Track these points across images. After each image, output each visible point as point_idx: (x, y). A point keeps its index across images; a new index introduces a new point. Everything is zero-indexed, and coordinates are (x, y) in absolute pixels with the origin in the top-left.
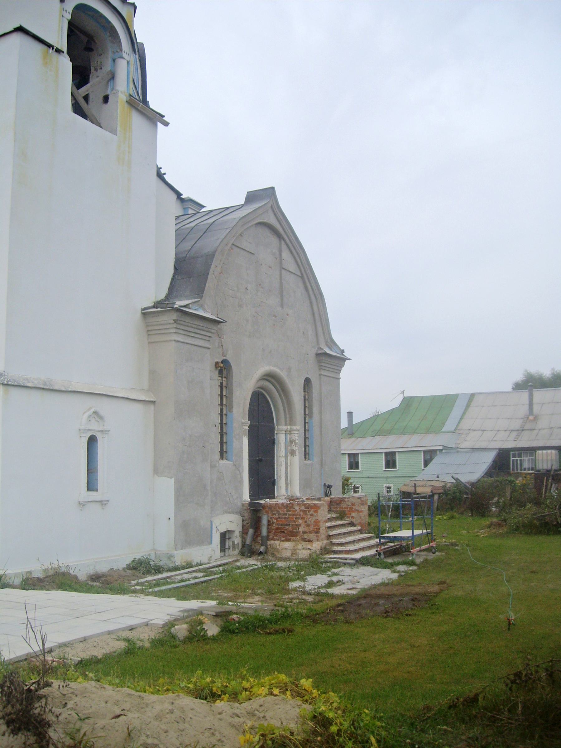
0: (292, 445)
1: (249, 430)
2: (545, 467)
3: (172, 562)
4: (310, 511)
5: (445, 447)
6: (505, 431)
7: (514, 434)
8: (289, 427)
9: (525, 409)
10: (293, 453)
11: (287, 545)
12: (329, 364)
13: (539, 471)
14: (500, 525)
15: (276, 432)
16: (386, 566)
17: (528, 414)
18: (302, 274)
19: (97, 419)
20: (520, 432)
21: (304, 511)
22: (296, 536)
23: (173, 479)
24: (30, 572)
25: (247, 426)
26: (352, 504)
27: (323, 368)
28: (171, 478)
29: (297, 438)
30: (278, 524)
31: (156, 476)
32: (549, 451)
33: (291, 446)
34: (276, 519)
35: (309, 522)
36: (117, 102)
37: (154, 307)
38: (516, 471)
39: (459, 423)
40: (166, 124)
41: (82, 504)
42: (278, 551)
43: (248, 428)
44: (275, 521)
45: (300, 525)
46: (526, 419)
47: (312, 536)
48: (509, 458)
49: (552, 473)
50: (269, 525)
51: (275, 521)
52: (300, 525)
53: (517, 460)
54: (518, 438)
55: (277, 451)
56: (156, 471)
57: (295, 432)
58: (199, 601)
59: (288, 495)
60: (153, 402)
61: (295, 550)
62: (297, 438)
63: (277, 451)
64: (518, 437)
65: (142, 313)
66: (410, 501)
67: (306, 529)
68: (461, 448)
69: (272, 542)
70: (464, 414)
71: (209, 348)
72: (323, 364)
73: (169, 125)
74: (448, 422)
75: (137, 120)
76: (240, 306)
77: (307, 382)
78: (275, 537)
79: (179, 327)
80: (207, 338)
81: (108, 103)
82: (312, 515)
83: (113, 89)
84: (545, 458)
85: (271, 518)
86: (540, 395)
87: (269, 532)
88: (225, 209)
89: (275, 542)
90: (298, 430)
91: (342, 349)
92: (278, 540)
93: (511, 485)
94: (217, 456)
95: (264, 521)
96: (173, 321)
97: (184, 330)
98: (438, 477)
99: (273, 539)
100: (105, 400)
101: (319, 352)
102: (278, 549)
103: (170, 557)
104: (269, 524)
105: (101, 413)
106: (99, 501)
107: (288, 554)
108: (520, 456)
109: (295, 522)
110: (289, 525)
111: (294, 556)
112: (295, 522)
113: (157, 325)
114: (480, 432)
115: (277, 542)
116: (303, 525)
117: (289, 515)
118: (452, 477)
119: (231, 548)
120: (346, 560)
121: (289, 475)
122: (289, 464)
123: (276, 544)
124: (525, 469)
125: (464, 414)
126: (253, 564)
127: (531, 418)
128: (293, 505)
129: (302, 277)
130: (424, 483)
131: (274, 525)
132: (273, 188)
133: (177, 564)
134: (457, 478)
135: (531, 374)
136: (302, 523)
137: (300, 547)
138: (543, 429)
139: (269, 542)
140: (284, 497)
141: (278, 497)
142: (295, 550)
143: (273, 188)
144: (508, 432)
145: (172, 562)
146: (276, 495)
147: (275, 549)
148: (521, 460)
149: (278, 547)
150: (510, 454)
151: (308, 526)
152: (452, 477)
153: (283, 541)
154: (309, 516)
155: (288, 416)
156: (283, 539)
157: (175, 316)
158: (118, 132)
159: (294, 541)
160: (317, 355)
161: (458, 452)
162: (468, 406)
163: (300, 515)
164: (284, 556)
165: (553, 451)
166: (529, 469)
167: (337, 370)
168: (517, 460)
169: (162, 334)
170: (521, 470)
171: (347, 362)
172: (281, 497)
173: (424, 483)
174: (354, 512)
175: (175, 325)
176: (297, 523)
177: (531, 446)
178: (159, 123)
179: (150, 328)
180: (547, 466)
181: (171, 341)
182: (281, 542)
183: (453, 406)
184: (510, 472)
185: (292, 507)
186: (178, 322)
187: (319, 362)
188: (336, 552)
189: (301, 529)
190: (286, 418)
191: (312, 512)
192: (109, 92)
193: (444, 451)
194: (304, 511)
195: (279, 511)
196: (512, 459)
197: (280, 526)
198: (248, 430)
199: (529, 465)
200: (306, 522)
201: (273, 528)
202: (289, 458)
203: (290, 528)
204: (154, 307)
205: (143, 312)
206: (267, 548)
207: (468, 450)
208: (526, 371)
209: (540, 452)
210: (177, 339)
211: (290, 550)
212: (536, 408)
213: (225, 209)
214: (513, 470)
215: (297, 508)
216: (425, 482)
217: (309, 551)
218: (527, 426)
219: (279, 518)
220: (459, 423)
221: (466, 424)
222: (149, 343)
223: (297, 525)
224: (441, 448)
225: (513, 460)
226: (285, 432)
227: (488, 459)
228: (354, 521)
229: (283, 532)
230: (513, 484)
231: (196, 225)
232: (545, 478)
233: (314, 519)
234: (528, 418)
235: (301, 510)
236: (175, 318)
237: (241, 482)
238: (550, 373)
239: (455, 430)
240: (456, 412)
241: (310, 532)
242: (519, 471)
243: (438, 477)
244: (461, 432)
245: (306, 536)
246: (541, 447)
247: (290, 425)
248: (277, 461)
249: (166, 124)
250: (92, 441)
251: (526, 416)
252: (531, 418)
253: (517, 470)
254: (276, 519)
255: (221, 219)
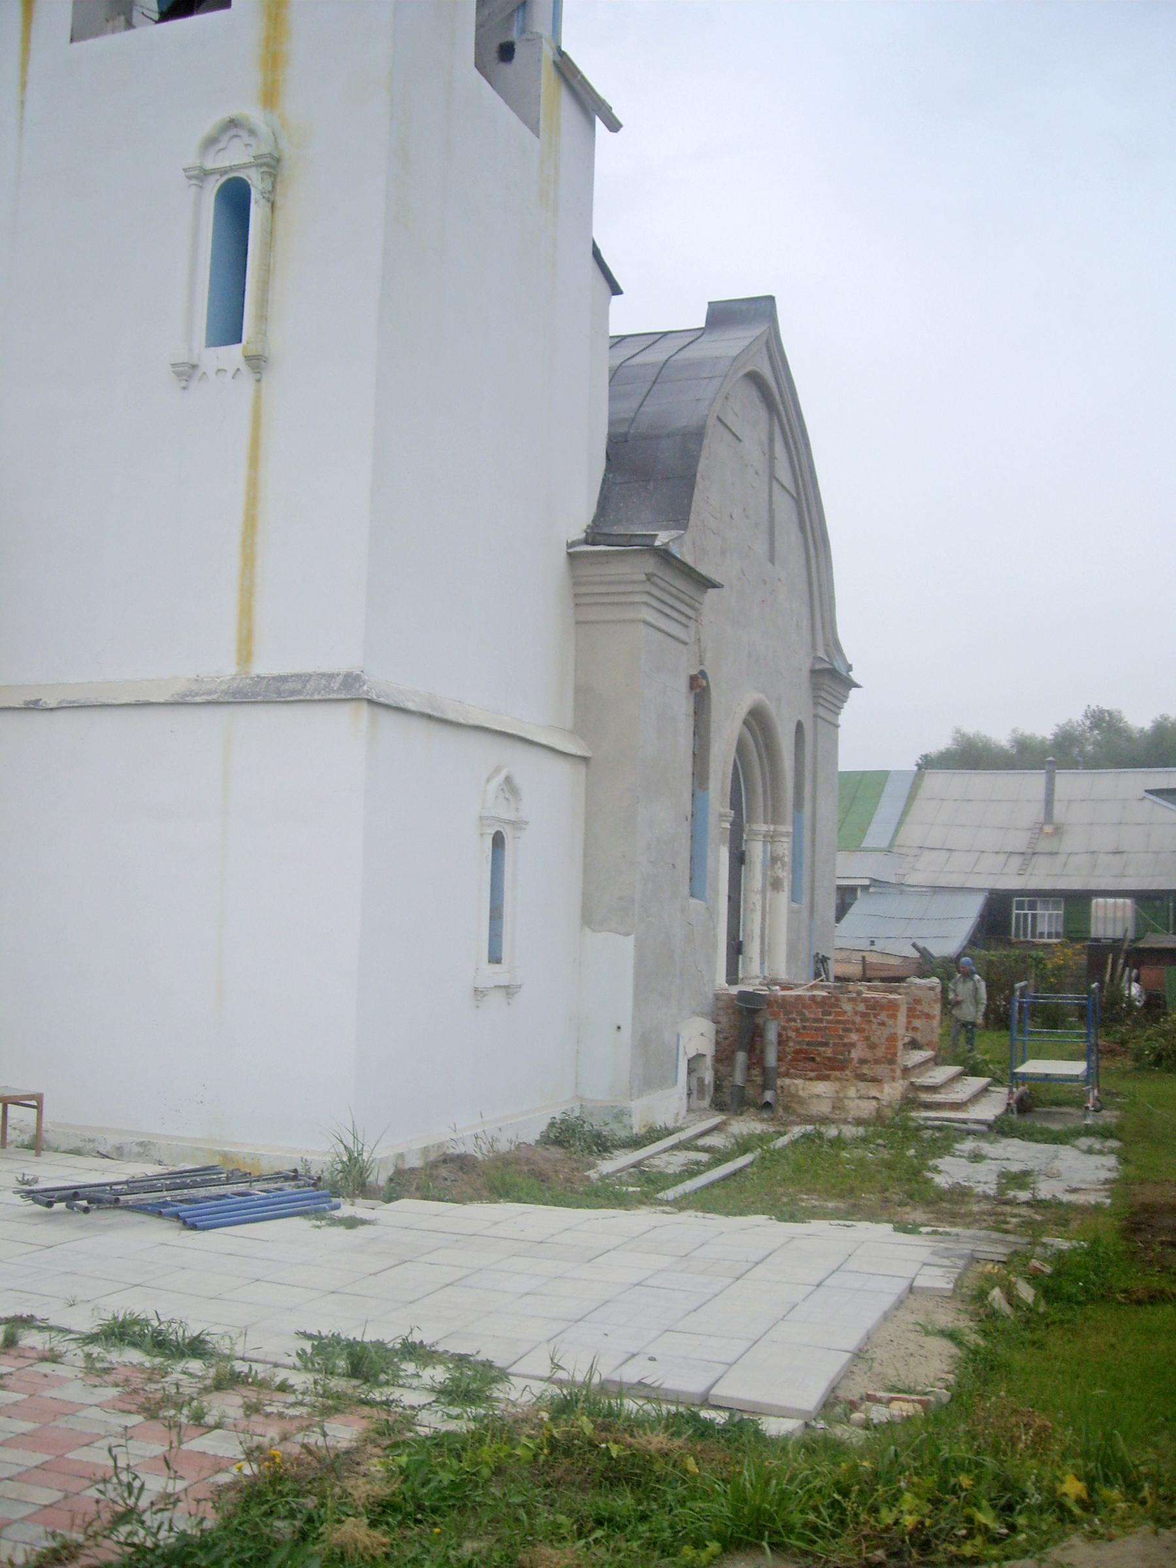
0: (776, 867)
1: (731, 830)
2: (1110, 933)
3: (625, 1127)
4: (878, 1015)
5: (876, 881)
6: (997, 853)
7: (1016, 862)
8: (772, 828)
9: (1035, 812)
10: (776, 884)
11: (821, 1087)
12: (832, 695)
13: (1097, 940)
14: (1112, 1053)
15: (745, 837)
16: (1054, 1139)
17: (1042, 820)
18: (798, 493)
19: (508, 795)
20: (1028, 857)
21: (863, 1015)
22: (842, 1069)
23: (632, 937)
24: (401, 1156)
25: (727, 821)
26: (914, 1000)
27: (822, 701)
28: (627, 934)
29: (786, 852)
30: (799, 1043)
31: (587, 930)
32: (1120, 901)
33: (772, 868)
34: (797, 1030)
35: (874, 1039)
36: (539, 60)
37: (586, 542)
38: (1022, 939)
39: (897, 831)
40: (614, 125)
41: (479, 993)
42: (801, 1101)
43: (729, 827)
44: (793, 1034)
45: (853, 1045)
46: (1038, 830)
47: (881, 1070)
48: (1011, 910)
49: (1126, 946)
50: (780, 1043)
51: (793, 1034)
52: (853, 1045)
53: (1026, 915)
54: (1025, 870)
55: (746, 877)
56: (588, 918)
57: (783, 839)
58: (832, 1222)
59: (765, 978)
60: (585, 760)
61: (841, 1100)
62: (786, 852)
63: (746, 877)
64: (1024, 867)
65: (569, 554)
66: (1085, 999)
67: (868, 1054)
68: (909, 886)
69: (787, 1081)
70: (904, 813)
71: (685, 643)
72: (823, 694)
73: (622, 129)
74: (873, 828)
75: (567, 110)
76: (723, 553)
77: (799, 727)
78: (792, 1071)
79: (655, 591)
80: (683, 619)
81: (515, 61)
82: (883, 1024)
83: (523, 31)
84: (1110, 914)
85: (784, 1028)
86: (1069, 783)
87: (780, 1059)
88: (658, 337)
89: (796, 1082)
90: (786, 834)
91: (850, 662)
92: (799, 1077)
93: (1037, 967)
94: (685, 889)
95: (771, 1035)
96: (644, 577)
97: (658, 599)
98: (872, 943)
99: (787, 1075)
100: (520, 750)
101: (818, 666)
102: (800, 1096)
103: (620, 1115)
104: (782, 1041)
105: (518, 781)
106: (504, 986)
107: (825, 1108)
108: (1032, 906)
109: (841, 1037)
110: (826, 1044)
111: (837, 1112)
112: (841, 1037)
113: (601, 583)
114: (945, 854)
115: (799, 1082)
116: (860, 1045)
117: (829, 1022)
118: (914, 945)
119: (695, 1092)
120: (966, 1123)
121: (767, 932)
122: (768, 909)
123: (796, 1086)
124: (1041, 935)
125: (904, 813)
126: (688, 1127)
127: (1048, 829)
128: (837, 1000)
129: (797, 501)
130: (844, 955)
131: (791, 1044)
132: (771, 299)
133: (635, 1131)
134: (924, 948)
135: (970, 738)
136: (859, 1040)
137: (852, 1092)
138: (1077, 854)
139: (779, 1082)
140: (757, 981)
141: (746, 982)
142: (841, 1100)
143: (771, 299)
144: (1002, 857)
145: (625, 1127)
146: (740, 976)
147: (795, 1097)
148: (1034, 916)
149: (801, 1093)
150: (1011, 902)
151: (873, 1047)
152: (914, 945)
153: (810, 1079)
154: (874, 1027)
155: (769, 803)
156: (812, 1074)
157: (650, 564)
158: (541, 133)
159: (837, 1079)
160: (814, 672)
161: (902, 892)
162: (912, 797)
163: (853, 1023)
164: (814, 1113)
165: (1128, 901)
166: (1050, 936)
167: (834, 705)
168: (1026, 915)
169: (613, 604)
170: (1033, 936)
171: (853, 692)
172: (751, 981)
173: (844, 955)
174: (919, 1017)
175: (648, 587)
176: (846, 1041)
177: (1058, 888)
178: (598, 121)
179: (583, 590)
180: (1114, 931)
181: (633, 621)
182: (808, 1083)
183: (879, 796)
184: (1010, 940)
185: (836, 1006)
186: (656, 579)
187: (816, 688)
188: (928, 1106)
189: (855, 1054)
190: (765, 807)
191: (883, 1016)
192: (514, 36)
193: (872, 890)
194: (864, 1015)
195: (804, 1014)
196: (1015, 912)
197: (805, 1047)
198: (728, 832)
199: (1050, 925)
200: (867, 1038)
201: (787, 1049)
202: (768, 895)
203: (829, 1052)
204: (586, 542)
205: (571, 550)
206: (777, 1094)
207: (924, 889)
208: (958, 731)
209: (1101, 900)
210: (649, 619)
211: (827, 1100)
212: (1058, 811)
213: (658, 337)
214: (1017, 935)
215: (848, 1007)
216: (848, 953)
217: (874, 1103)
218: (1043, 845)
219: (804, 1028)
220: (897, 831)
221: (913, 834)
222: (577, 623)
223: (845, 1045)
224: (867, 882)
225: (1018, 916)
226: (764, 837)
227: (970, 910)
228: (918, 1036)
229: (813, 1059)
230: (1041, 966)
231: (620, 365)
232: (1111, 956)
233: (886, 1032)
234: (1041, 829)
235: (856, 1013)
236: (649, 570)
237: (714, 947)
238: (1009, 737)
239: (891, 845)
240: (888, 808)
241: (877, 1062)
242: (1029, 938)
243: (872, 943)
244: (903, 851)
245: (865, 1070)
246: (1111, 891)
247: (774, 822)
248: (745, 902)
249: (614, 125)
250: (498, 841)
251: (1038, 826)
252: (1048, 829)
253: (1025, 935)
254: (797, 1030)
255: (677, 357)
